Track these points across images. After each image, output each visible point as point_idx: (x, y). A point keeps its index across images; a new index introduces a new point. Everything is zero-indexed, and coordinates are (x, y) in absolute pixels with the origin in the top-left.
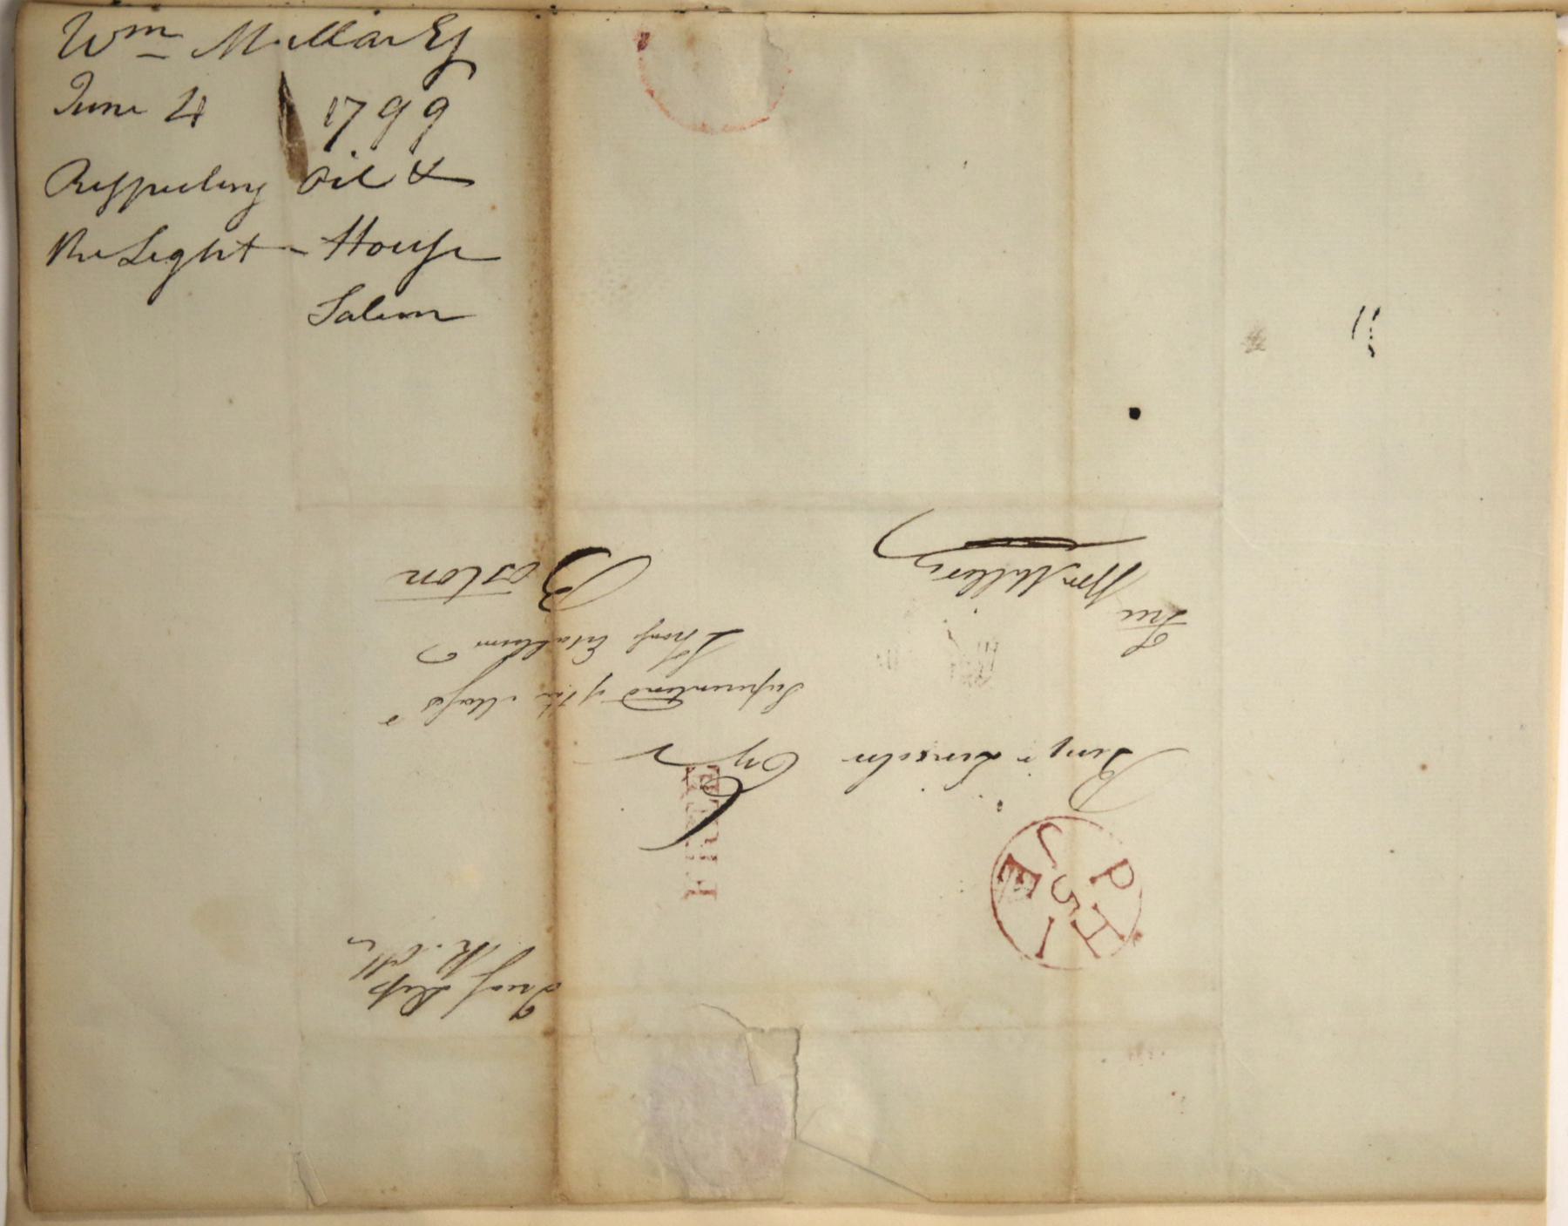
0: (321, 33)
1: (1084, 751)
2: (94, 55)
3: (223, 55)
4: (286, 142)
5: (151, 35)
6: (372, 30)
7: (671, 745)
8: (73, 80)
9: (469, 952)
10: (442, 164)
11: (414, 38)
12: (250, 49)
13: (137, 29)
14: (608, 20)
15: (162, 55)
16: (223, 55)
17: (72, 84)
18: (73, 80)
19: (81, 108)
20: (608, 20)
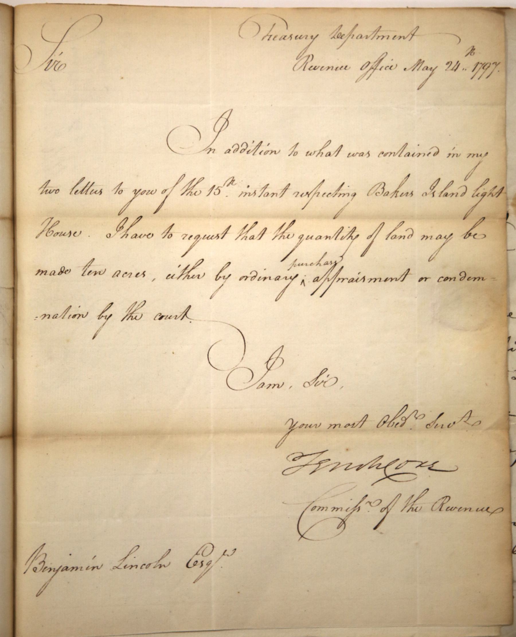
0: (278, 296)
1: (387, 278)
2: (197, 235)
3: (332, 469)
4: (481, 431)
5: (265, 280)
6: (398, 494)
7: (438, 462)
8: (284, 471)
9: (387, 195)
10: (438, 415)
11: (326, 466)
12: (348, 468)
13: (212, 149)
14: (190, 322)
15: (222, 285)
16: (332, 469)
17: (283, 473)
18: (284, 471)
19: (89, 568)
20: (190, 322)
